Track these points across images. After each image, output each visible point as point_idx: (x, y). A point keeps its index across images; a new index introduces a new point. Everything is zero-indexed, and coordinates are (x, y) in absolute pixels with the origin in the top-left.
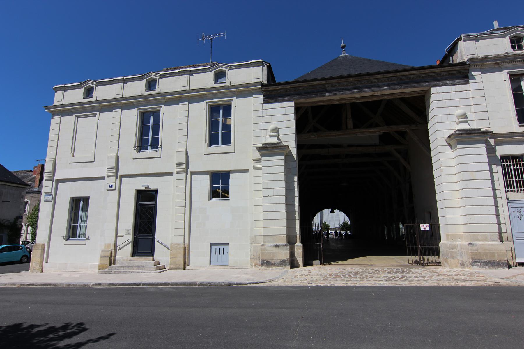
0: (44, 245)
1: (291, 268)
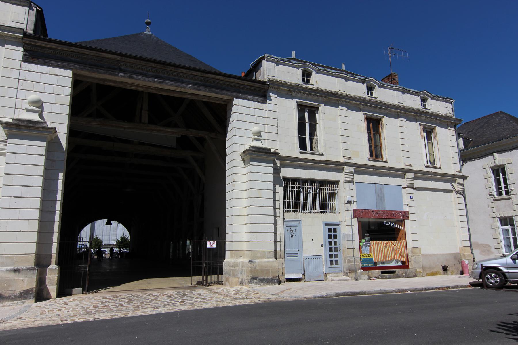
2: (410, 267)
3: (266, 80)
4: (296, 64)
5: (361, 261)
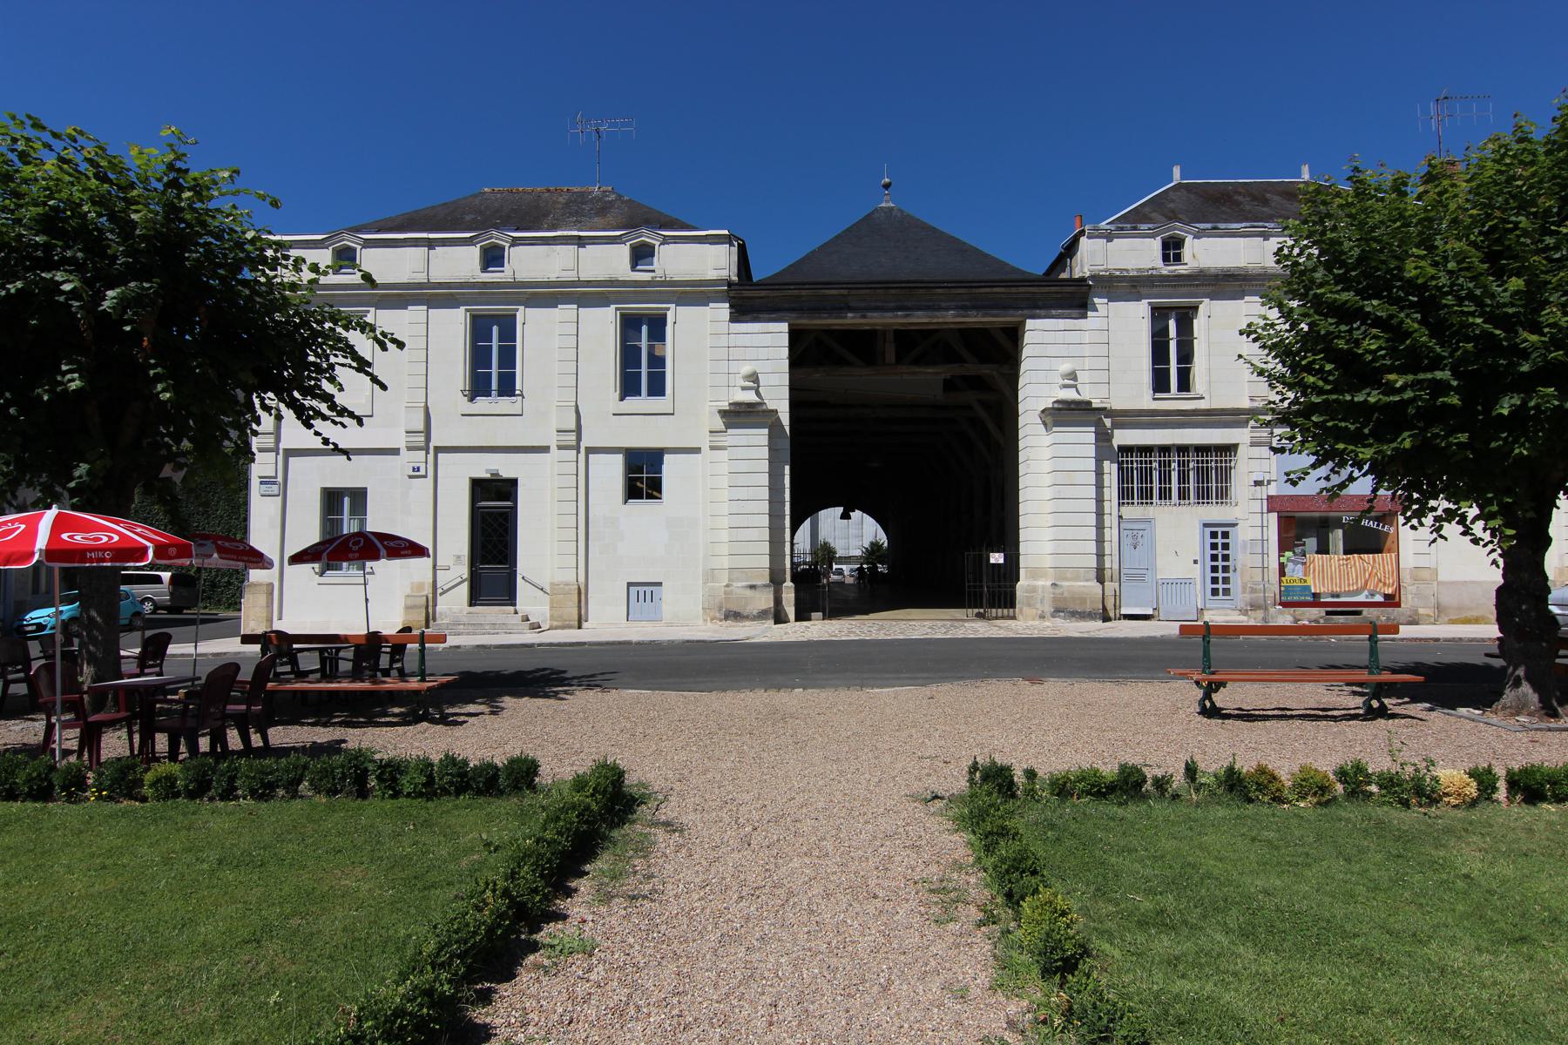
0: (271, 585)
1: (775, 623)
2: (1402, 605)
3: (1087, 275)
4: (1149, 229)
5: (1283, 589)
